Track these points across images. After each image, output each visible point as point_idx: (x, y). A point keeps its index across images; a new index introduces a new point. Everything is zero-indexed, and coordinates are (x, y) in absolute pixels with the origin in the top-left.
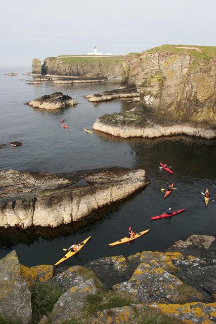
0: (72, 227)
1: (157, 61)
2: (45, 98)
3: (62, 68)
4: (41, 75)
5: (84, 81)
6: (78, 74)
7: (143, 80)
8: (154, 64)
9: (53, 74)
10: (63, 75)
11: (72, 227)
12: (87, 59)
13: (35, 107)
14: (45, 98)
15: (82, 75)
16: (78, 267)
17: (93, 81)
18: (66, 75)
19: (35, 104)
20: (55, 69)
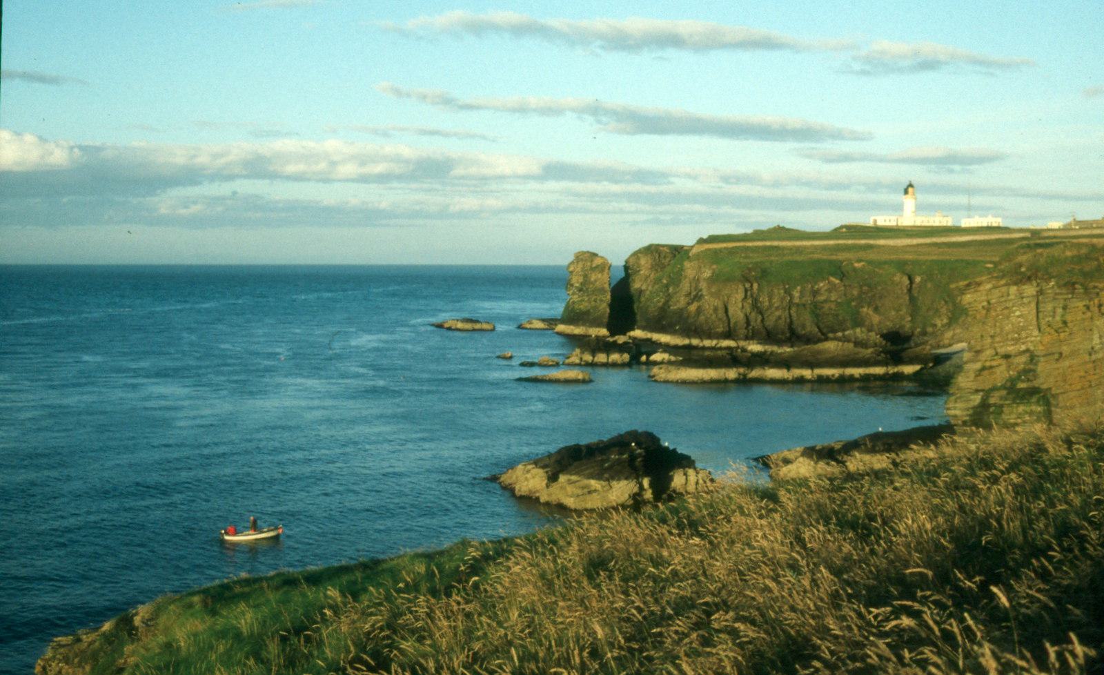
0: (235, 530)
1: (1032, 317)
2: (569, 460)
3: (710, 302)
4: (604, 332)
5: (807, 373)
6: (793, 336)
7: (977, 399)
8: (1019, 330)
9: (662, 329)
10: (710, 337)
11: (235, 530)
12: (841, 256)
13: (522, 497)
14: (569, 460)
15: (809, 340)
16: (269, 575)
17: (857, 372)
18: (728, 335)
19: (531, 480)
20: (679, 302)
